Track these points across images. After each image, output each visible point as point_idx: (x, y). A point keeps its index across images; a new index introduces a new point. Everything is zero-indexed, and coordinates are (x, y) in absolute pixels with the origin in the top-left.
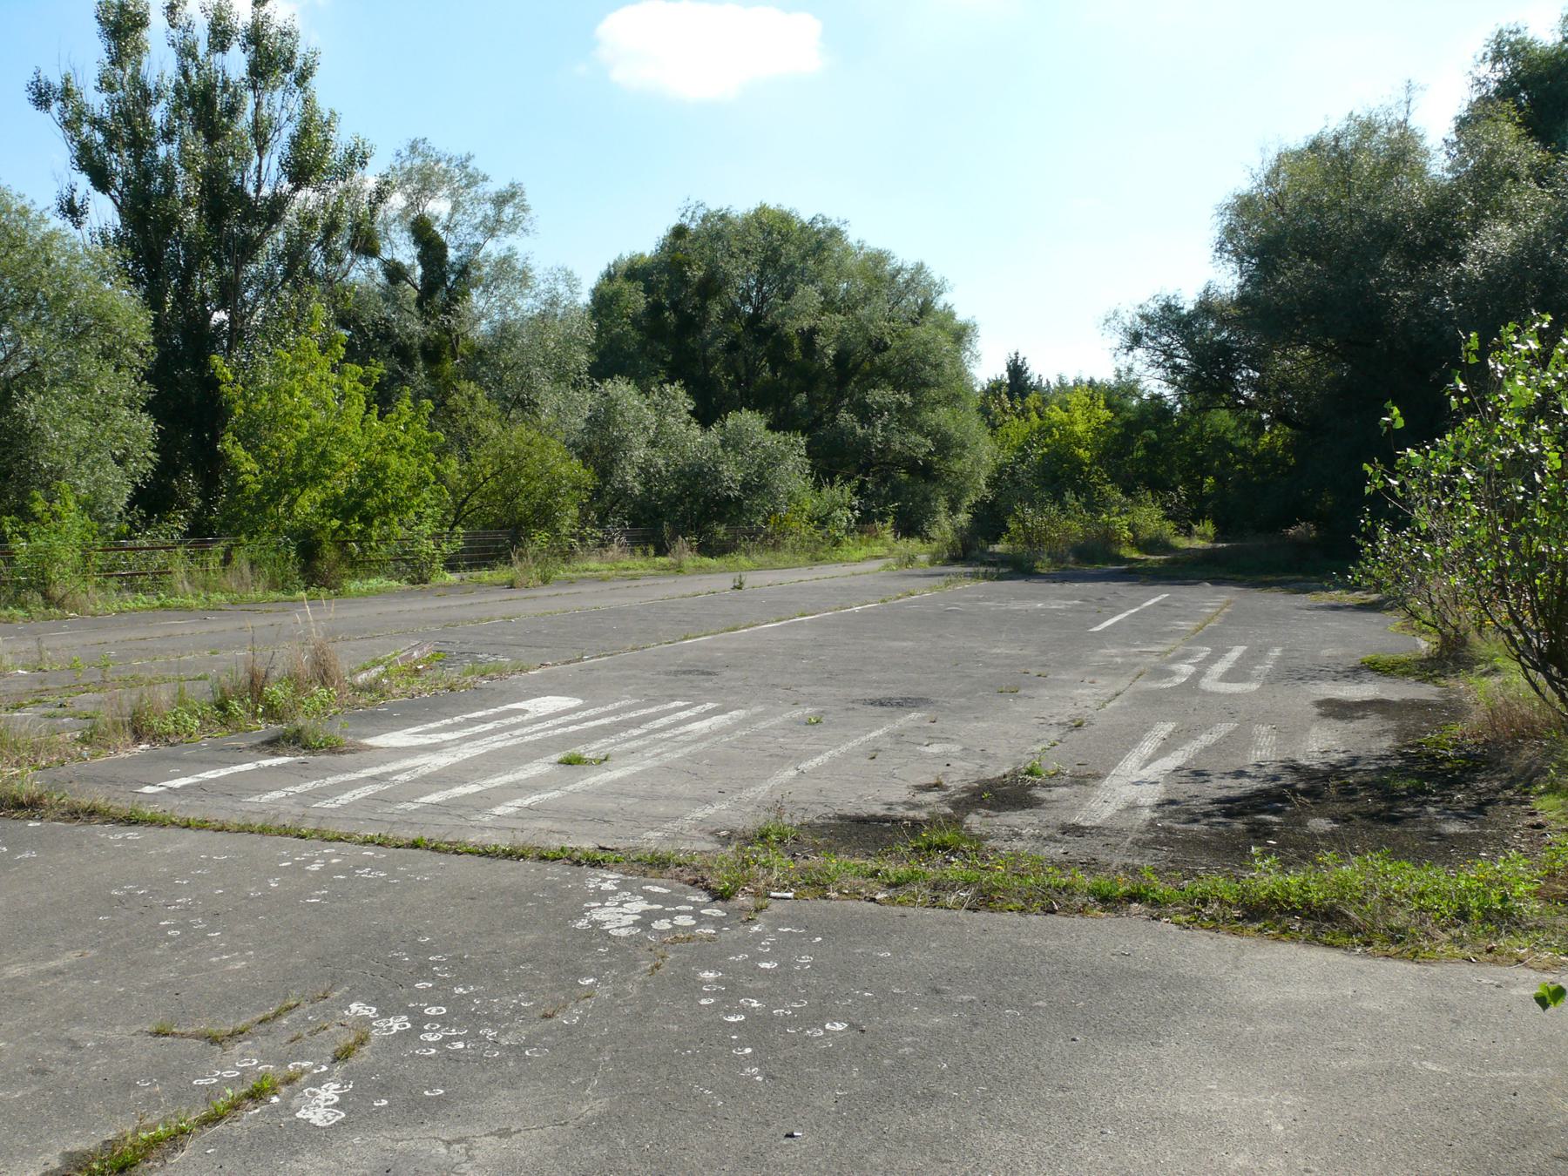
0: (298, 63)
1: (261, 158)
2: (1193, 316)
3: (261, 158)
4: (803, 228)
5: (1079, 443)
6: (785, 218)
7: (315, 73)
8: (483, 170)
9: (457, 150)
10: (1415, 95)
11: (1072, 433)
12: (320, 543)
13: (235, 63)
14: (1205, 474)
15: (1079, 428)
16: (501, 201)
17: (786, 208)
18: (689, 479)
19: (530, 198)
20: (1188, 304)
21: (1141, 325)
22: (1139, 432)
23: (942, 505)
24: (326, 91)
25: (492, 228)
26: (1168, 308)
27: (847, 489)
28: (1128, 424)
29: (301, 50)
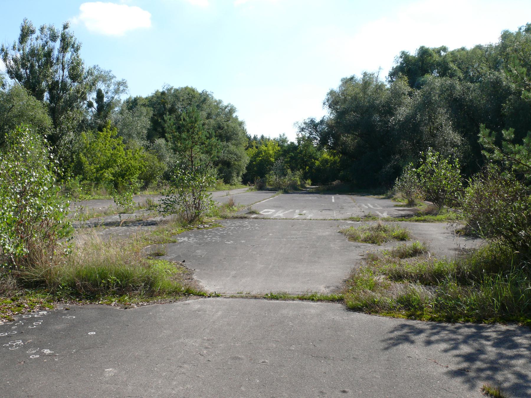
0: (76, 46)
1: (63, 72)
2: (318, 124)
3: (63, 72)
4: (200, 94)
5: (271, 156)
6: (193, 90)
7: (81, 49)
8: (115, 75)
9: (107, 69)
10: (381, 71)
11: (269, 153)
12: (118, 183)
13: (57, 45)
14: (306, 166)
15: (271, 152)
16: (119, 84)
17: (194, 87)
18: (440, 184)
19: (129, 84)
20: (318, 120)
21: (304, 126)
22: (288, 153)
23: (235, 174)
24: (83, 54)
25: (117, 91)
26: (312, 121)
27: (216, 170)
28: (285, 151)
29: (77, 42)
